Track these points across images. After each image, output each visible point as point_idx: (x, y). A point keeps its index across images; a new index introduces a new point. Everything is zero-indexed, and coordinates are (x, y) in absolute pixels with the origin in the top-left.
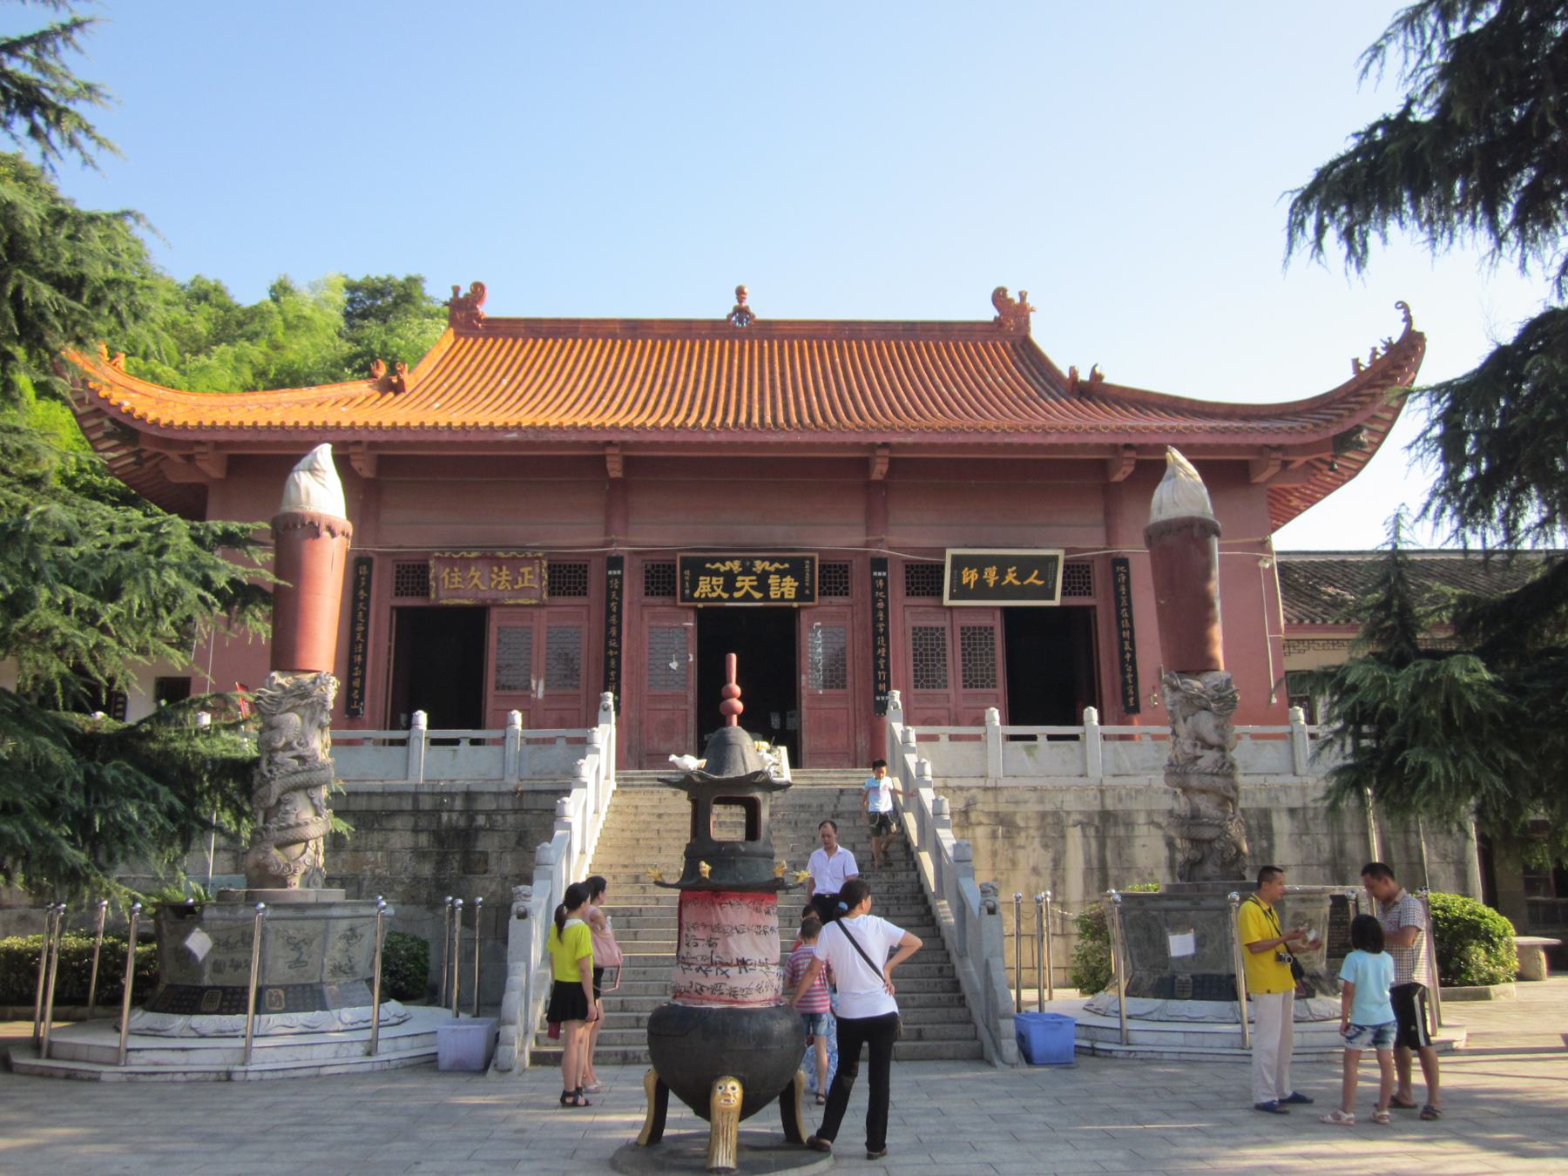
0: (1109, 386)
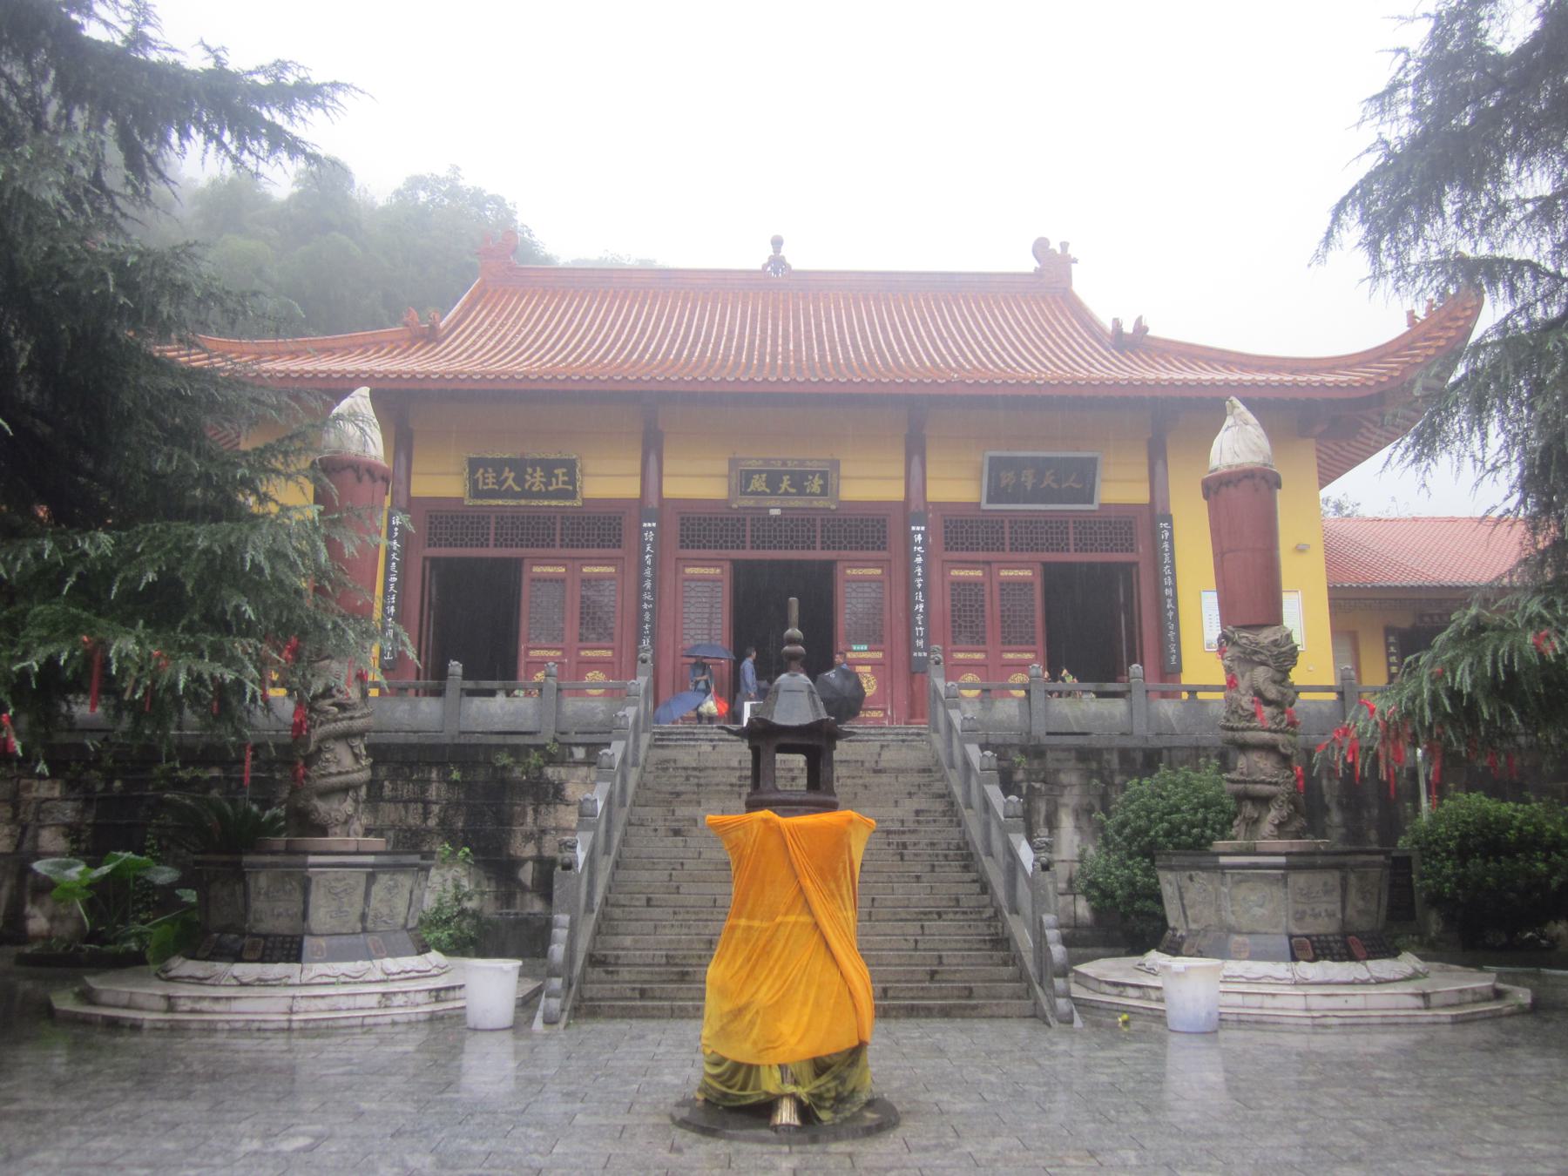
0: (1153, 339)
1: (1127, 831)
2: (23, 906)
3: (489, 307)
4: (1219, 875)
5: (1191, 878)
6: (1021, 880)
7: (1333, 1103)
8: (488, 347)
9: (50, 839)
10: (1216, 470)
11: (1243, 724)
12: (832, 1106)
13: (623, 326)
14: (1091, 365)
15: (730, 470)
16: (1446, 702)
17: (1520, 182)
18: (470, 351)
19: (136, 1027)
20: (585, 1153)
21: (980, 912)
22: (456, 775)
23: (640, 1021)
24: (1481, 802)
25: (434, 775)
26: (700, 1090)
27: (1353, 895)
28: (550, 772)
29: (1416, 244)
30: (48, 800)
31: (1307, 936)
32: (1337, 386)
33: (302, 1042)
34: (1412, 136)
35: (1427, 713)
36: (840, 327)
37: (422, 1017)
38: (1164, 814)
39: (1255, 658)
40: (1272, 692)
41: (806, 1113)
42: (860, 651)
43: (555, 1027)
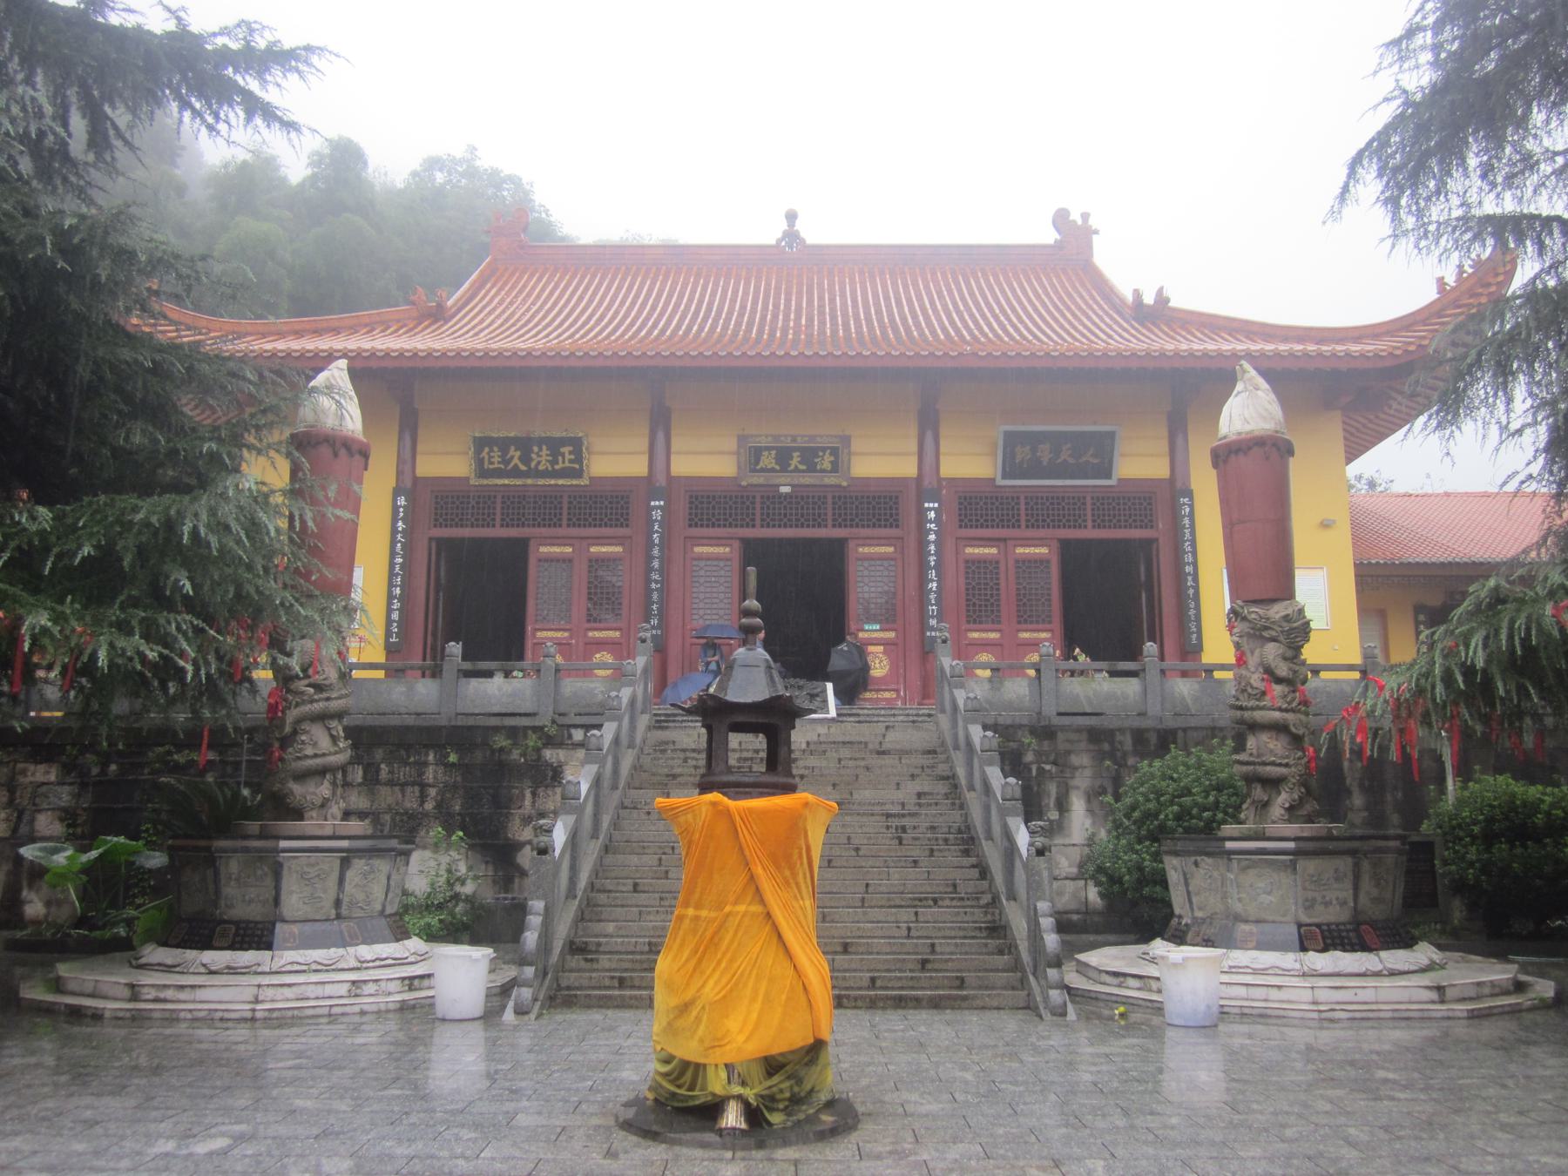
1: (1136, 814)
2: (19, 890)
3: (499, 285)
4: (1225, 861)
5: (1196, 864)
6: (1018, 864)
7: (1328, 1107)
8: (496, 325)
9: (46, 823)
10: (1225, 437)
11: (1252, 703)
12: (786, 1107)
13: (633, 303)
14: (1110, 337)
15: (739, 447)
16: (1460, 679)
17: (1549, 133)
18: (476, 330)
19: (97, 1016)
20: (514, 1158)
21: (978, 899)
22: (453, 758)
23: (617, 1011)
24: (1507, 785)
25: (431, 757)
26: (650, 1089)
27: (1366, 884)
28: (549, 754)
29: (1438, 199)
30: (44, 784)
31: (1318, 926)
32: (1363, 355)
33: (266, 1032)
34: (1434, 86)
35: (1439, 689)
36: (854, 301)
37: (391, 1006)
38: (1174, 797)
39: (1266, 634)
40: (1283, 670)
41: (754, 1116)
42: (871, 630)
43: (526, 1017)
